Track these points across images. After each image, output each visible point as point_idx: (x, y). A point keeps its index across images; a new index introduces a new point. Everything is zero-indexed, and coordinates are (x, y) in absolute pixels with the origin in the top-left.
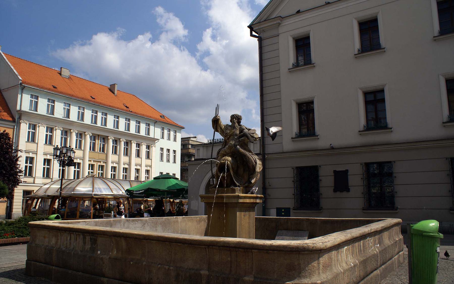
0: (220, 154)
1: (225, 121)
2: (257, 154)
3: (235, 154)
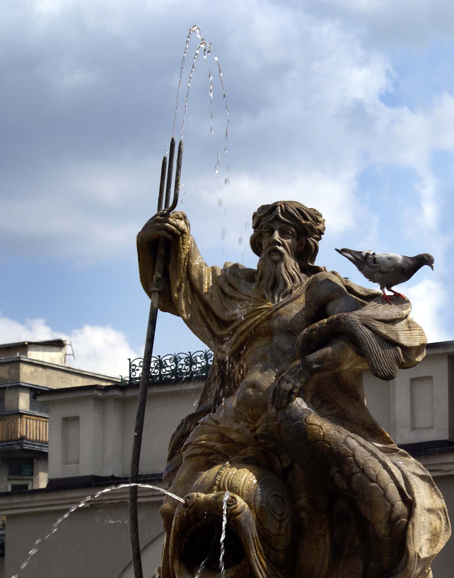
0: (191, 452)
1: (220, 240)
2: (417, 450)
3: (284, 453)
